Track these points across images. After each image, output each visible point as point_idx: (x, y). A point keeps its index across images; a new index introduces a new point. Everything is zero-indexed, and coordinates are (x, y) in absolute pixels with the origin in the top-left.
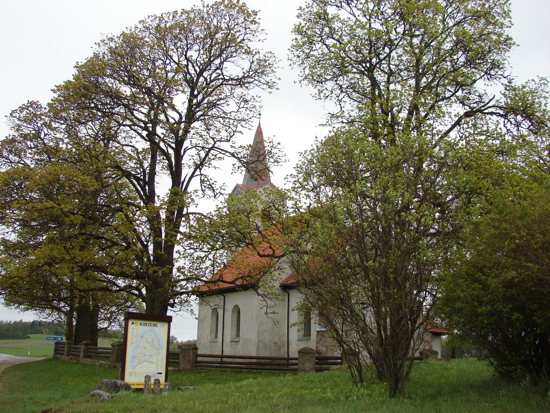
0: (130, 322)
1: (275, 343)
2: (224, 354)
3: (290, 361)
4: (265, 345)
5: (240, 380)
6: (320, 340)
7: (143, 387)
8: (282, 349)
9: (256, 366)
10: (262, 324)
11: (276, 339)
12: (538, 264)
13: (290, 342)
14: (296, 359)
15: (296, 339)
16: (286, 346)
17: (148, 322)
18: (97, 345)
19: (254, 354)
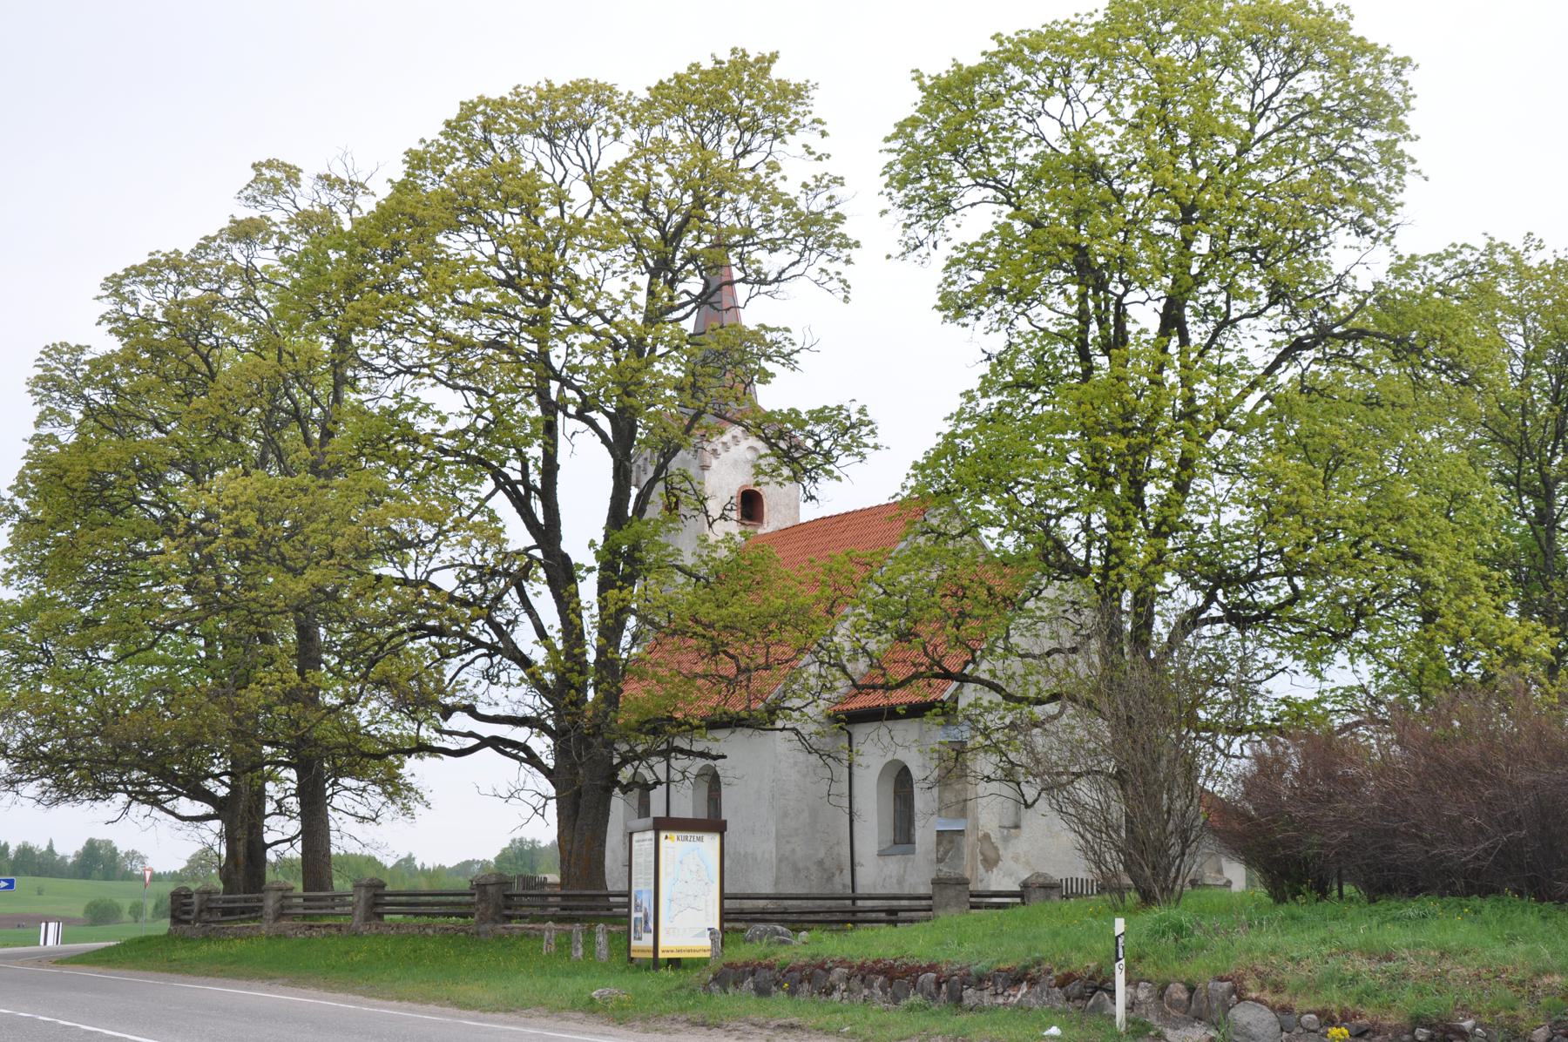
0: (663, 835)
1: (821, 863)
2: (860, 891)
3: (859, 903)
4: (796, 870)
5: (361, 1004)
6: (946, 853)
7: (708, 955)
8: (837, 879)
9: (883, 915)
10: (785, 815)
11: (821, 855)
12: (1334, 822)
13: (857, 859)
14: (930, 898)
15: (875, 849)
16: (847, 871)
17: (689, 834)
18: (603, 884)
19: (768, 889)
